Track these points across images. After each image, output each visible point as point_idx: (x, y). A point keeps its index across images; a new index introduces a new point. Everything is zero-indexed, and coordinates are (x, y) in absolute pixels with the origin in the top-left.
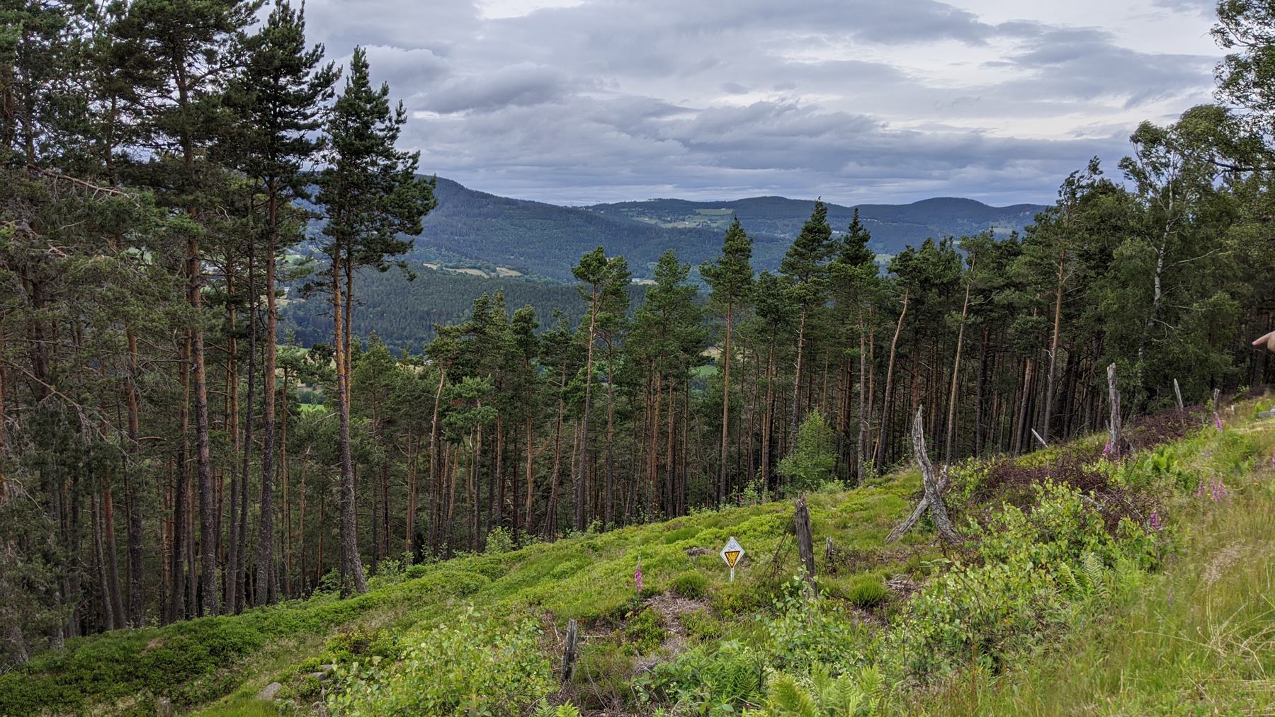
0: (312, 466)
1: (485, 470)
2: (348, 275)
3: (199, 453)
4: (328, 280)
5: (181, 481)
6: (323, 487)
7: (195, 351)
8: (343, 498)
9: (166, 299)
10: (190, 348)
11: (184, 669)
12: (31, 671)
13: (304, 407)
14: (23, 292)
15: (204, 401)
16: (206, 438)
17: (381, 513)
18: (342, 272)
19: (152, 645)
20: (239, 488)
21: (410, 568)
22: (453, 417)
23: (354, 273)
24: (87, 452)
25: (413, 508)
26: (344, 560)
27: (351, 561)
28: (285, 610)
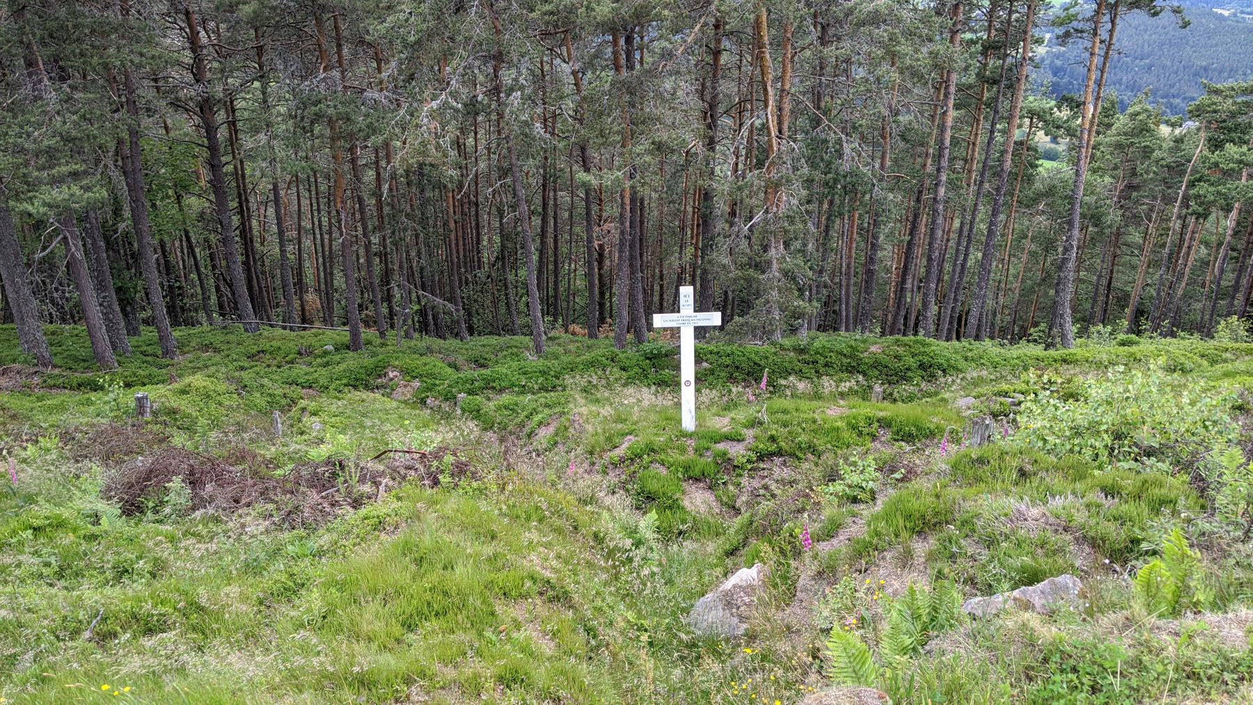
0: (1042, 221)
1: (1235, 254)
2: (1113, 22)
3: (936, 192)
4: (1088, 26)
5: (916, 216)
6: (1049, 246)
7: (946, 95)
8: (1064, 254)
9: (930, 40)
10: (943, 91)
11: (896, 375)
12: (782, 348)
13: (1048, 164)
14: (814, 34)
15: (947, 142)
16: (944, 178)
17: (1104, 282)
18: (1107, 18)
19: (873, 349)
20: (965, 233)
21: (1121, 336)
22: (1203, 188)
23: (1118, 21)
24: (845, 177)
25: (1138, 280)
26: (1054, 314)
27: (1062, 316)
28: (989, 347)
